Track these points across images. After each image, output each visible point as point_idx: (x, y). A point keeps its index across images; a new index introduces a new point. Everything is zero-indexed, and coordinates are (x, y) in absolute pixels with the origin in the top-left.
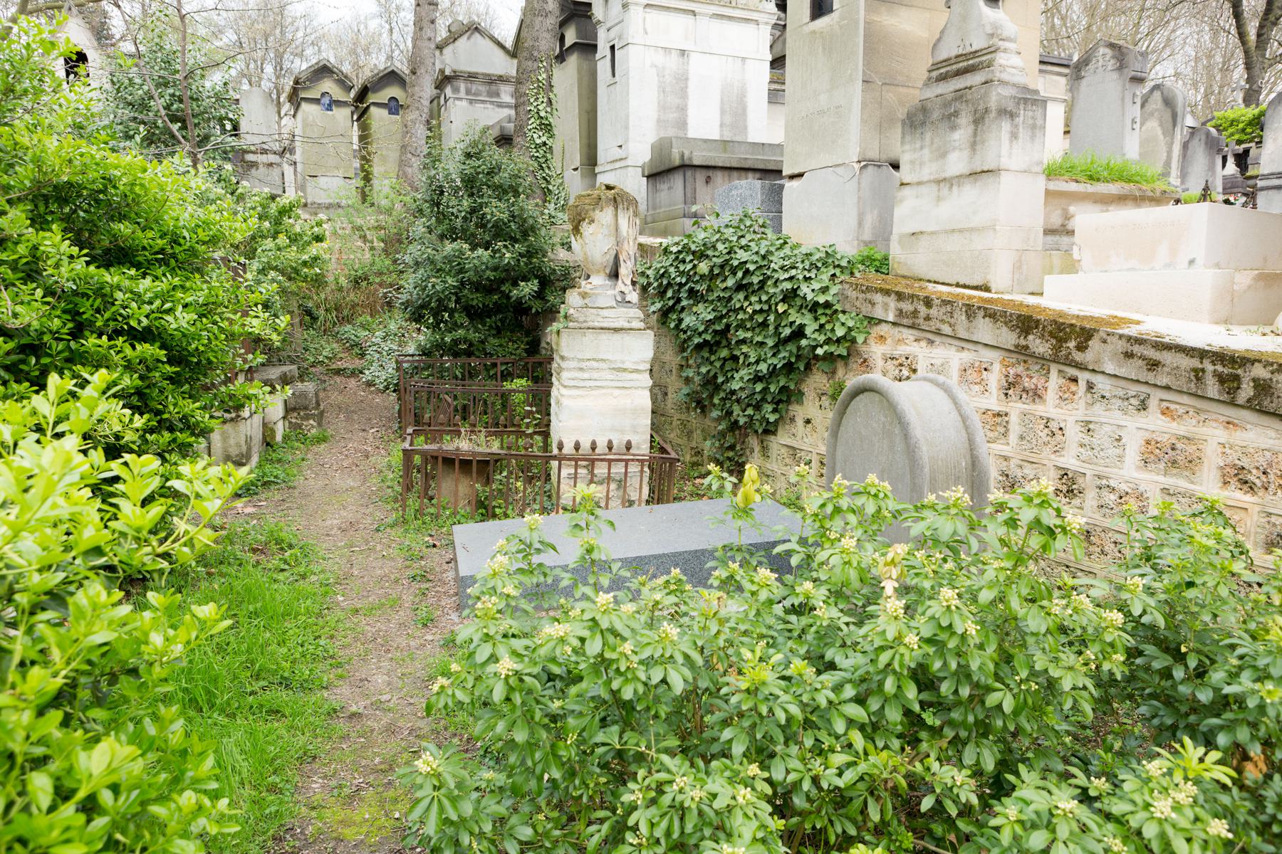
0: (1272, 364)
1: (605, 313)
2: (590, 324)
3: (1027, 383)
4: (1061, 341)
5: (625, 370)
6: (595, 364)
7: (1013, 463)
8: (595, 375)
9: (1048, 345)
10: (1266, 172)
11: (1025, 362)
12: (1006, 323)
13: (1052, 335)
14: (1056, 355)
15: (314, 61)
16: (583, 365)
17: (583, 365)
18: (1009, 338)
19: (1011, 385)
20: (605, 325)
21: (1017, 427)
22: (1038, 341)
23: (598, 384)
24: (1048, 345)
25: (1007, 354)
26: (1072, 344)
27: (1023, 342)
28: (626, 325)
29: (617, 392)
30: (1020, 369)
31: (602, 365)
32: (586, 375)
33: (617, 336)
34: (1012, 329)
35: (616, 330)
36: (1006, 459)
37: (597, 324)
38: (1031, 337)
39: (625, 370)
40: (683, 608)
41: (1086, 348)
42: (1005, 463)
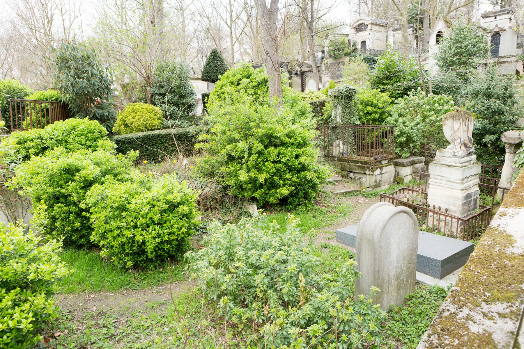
1: (446, 159)
2: (441, 163)
5: (451, 182)
6: (440, 178)
8: (440, 181)
10: (503, 56)
16: (436, 177)
17: (436, 177)
19: (223, 223)
20: (446, 164)
23: (441, 185)
28: (454, 164)
29: (448, 189)
31: (444, 179)
32: (437, 181)
33: (449, 168)
35: (449, 166)
37: (443, 163)
39: (451, 182)
40: (250, 271)
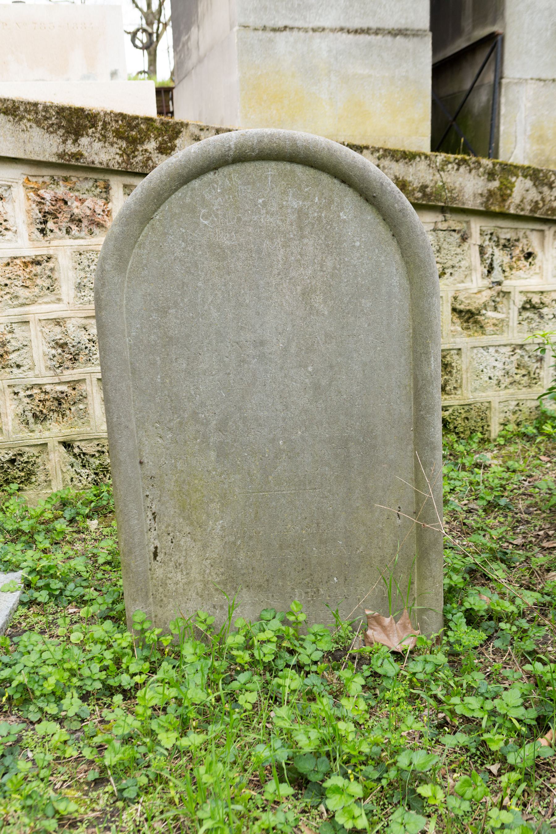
0: (378, 150)
3: (76, 208)
4: (134, 142)
7: (71, 326)
9: (114, 150)
11: (66, 179)
12: (38, 123)
13: (119, 135)
14: (128, 162)
15: (100, 791)
18: (45, 145)
19: (46, 216)
21: (71, 274)
22: (97, 145)
24: (114, 150)
25: (33, 171)
26: (151, 145)
27: (71, 148)
30: (61, 191)
34: (51, 130)
36: (58, 322)
38: (84, 141)
41: (173, 148)
42: (58, 329)
